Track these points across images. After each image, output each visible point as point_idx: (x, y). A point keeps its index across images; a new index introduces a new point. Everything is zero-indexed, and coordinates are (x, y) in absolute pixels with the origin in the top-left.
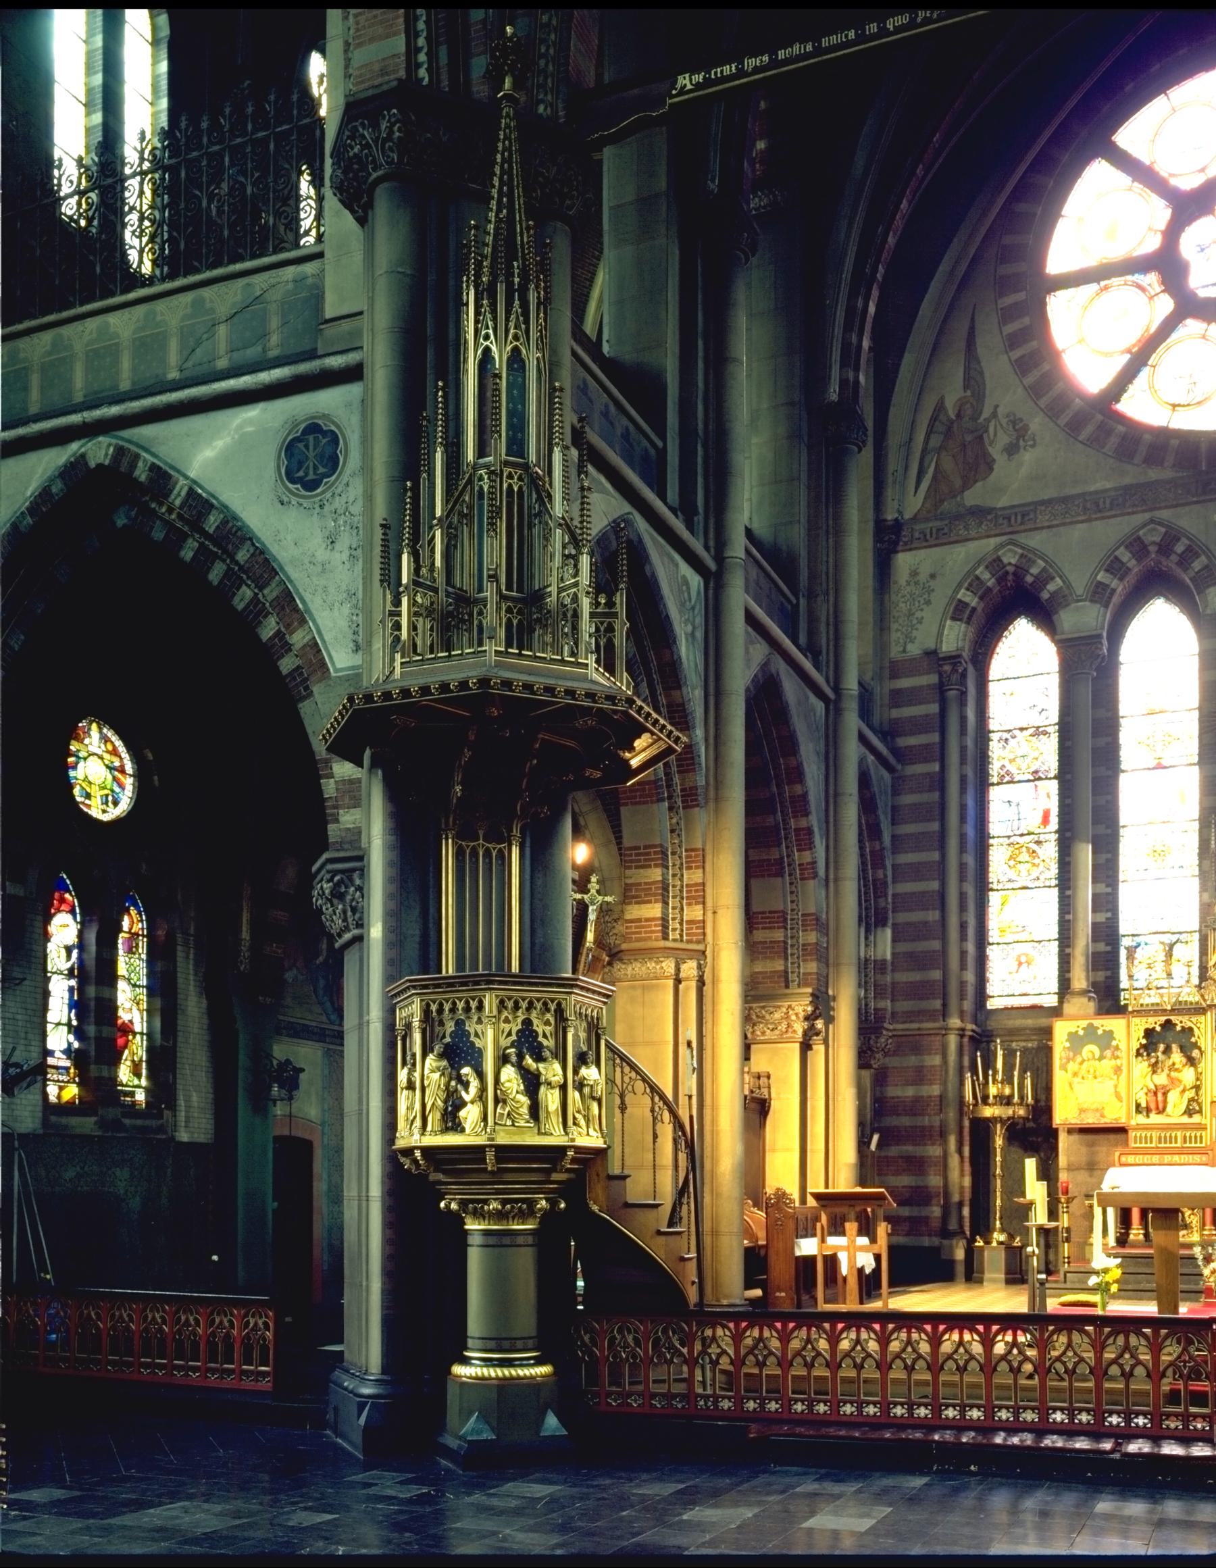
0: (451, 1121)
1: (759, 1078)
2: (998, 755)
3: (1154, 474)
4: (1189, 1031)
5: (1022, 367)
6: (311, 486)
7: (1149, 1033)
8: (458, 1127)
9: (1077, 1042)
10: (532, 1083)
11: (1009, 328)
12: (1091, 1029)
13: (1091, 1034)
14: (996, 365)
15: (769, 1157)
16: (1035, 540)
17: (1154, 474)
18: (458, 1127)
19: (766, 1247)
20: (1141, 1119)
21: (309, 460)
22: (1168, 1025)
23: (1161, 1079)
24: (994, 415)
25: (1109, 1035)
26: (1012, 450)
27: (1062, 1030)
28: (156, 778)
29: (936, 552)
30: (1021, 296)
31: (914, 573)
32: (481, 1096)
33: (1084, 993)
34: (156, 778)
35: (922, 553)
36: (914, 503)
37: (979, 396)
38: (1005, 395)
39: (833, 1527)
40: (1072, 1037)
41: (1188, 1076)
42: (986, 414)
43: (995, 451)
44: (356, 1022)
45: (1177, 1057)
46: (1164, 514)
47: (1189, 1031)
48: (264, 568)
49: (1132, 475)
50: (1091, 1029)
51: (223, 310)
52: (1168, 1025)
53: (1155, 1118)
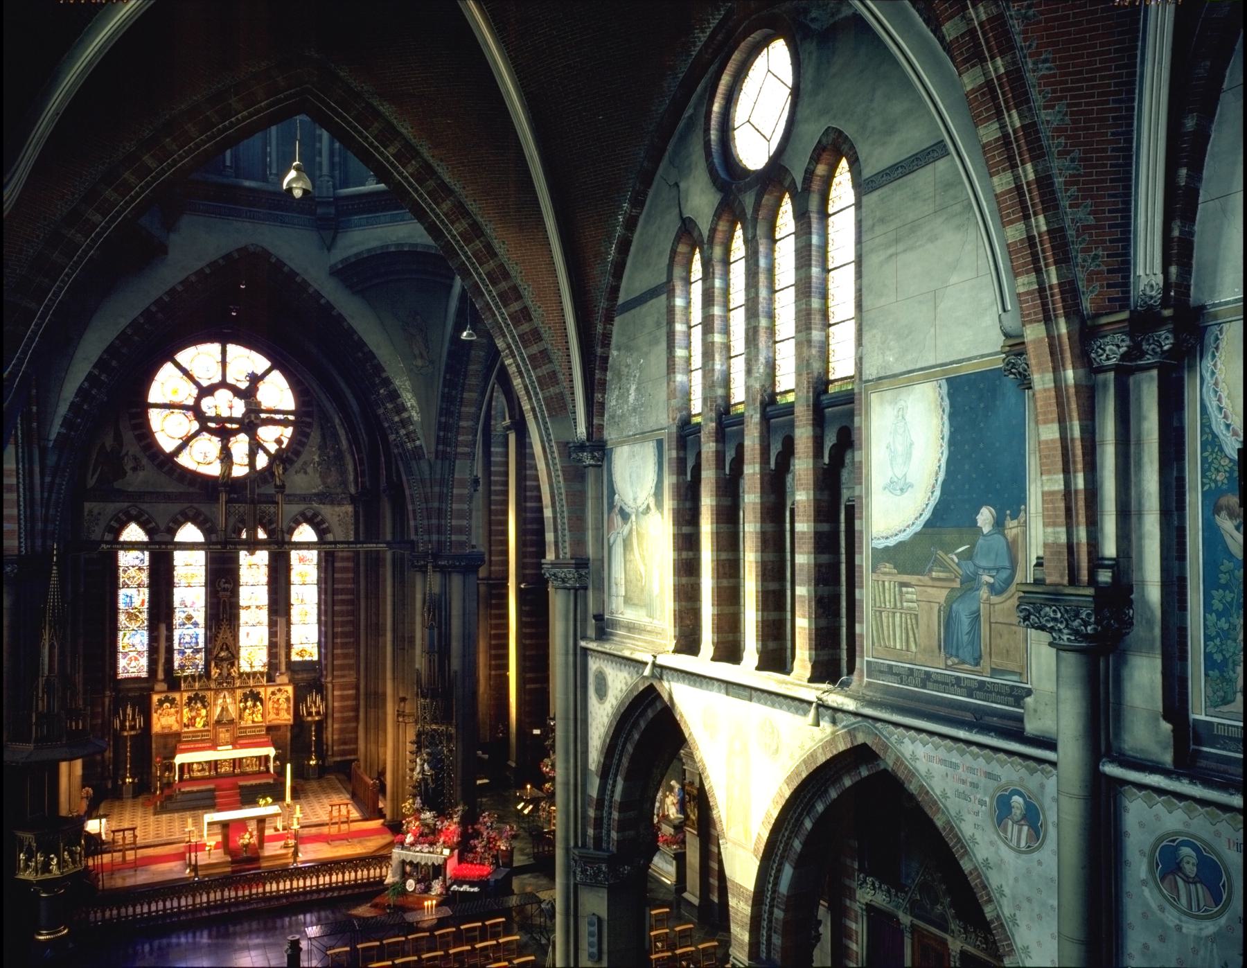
2: (123, 577)
3: (191, 490)
7: (189, 698)
8: (50, 872)
9: (161, 702)
11: (133, 422)
13: (167, 699)
14: (128, 436)
15: (811, 466)
16: (144, 506)
17: (191, 490)
19: (991, 175)
22: (196, 695)
23: (194, 714)
24: (127, 454)
25: (174, 699)
26: (134, 469)
28: (479, 782)
29: (102, 505)
32: (58, 863)
33: (163, 681)
34: (479, 782)
35: (94, 504)
36: (91, 482)
37: (121, 445)
38: (131, 447)
40: (159, 700)
41: (204, 712)
42: (124, 452)
43: (128, 468)
44: (1061, 706)
45: (199, 705)
46: (196, 505)
47: (204, 697)
49: (182, 488)
53: (191, 729)
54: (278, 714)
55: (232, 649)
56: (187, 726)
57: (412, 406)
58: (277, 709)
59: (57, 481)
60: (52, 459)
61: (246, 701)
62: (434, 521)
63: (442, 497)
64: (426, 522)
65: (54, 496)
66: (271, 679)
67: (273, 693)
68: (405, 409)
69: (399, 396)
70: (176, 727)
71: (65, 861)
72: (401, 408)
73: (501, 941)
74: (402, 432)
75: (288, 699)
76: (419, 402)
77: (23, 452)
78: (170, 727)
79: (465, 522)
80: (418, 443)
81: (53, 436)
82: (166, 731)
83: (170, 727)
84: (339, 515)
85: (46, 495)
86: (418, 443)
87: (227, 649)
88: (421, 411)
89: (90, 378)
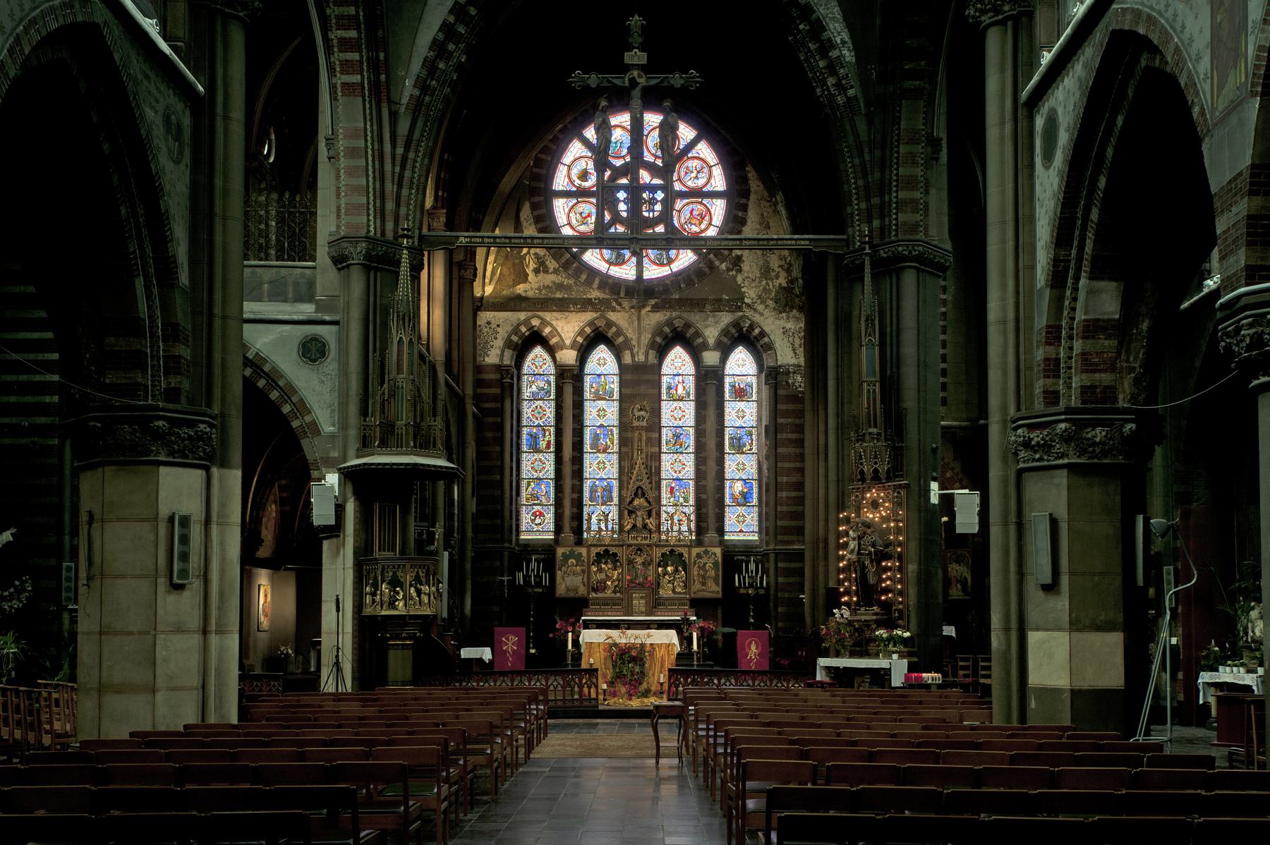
0: (392, 604)
1: (881, 556)
4: (615, 555)
5: (538, 220)
6: (314, 361)
8: (395, 608)
10: (419, 592)
12: (572, 552)
18: (395, 608)
20: (593, 595)
21: (312, 351)
27: (560, 551)
30: (542, 198)
31: (489, 323)
32: (404, 597)
39: (708, 431)
48: (288, 392)
50: (572, 552)
51: (266, 278)
52: (606, 551)
54: (704, 584)
55: (651, 495)
56: (596, 590)
57: (843, 42)
58: (703, 577)
59: (411, 155)
60: (404, 126)
61: (665, 566)
62: (876, 201)
63: (883, 165)
64: (863, 205)
65: (407, 174)
66: (699, 543)
67: (699, 556)
68: (831, 45)
69: (824, 29)
70: (582, 591)
71: (412, 598)
72: (826, 47)
73: (864, 348)
74: (831, 81)
75: (715, 564)
76: (852, 37)
77: (371, 108)
78: (576, 590)
79: (917, 195)
80: (851, 92)
81: (405, 101)
82: (572, 594)
83: (576, 590)
84: (785, 336)
85: (397, 169)
86: (851, 92)
87: (643, 494)
88: (857, 48)
89: (446, 28)
